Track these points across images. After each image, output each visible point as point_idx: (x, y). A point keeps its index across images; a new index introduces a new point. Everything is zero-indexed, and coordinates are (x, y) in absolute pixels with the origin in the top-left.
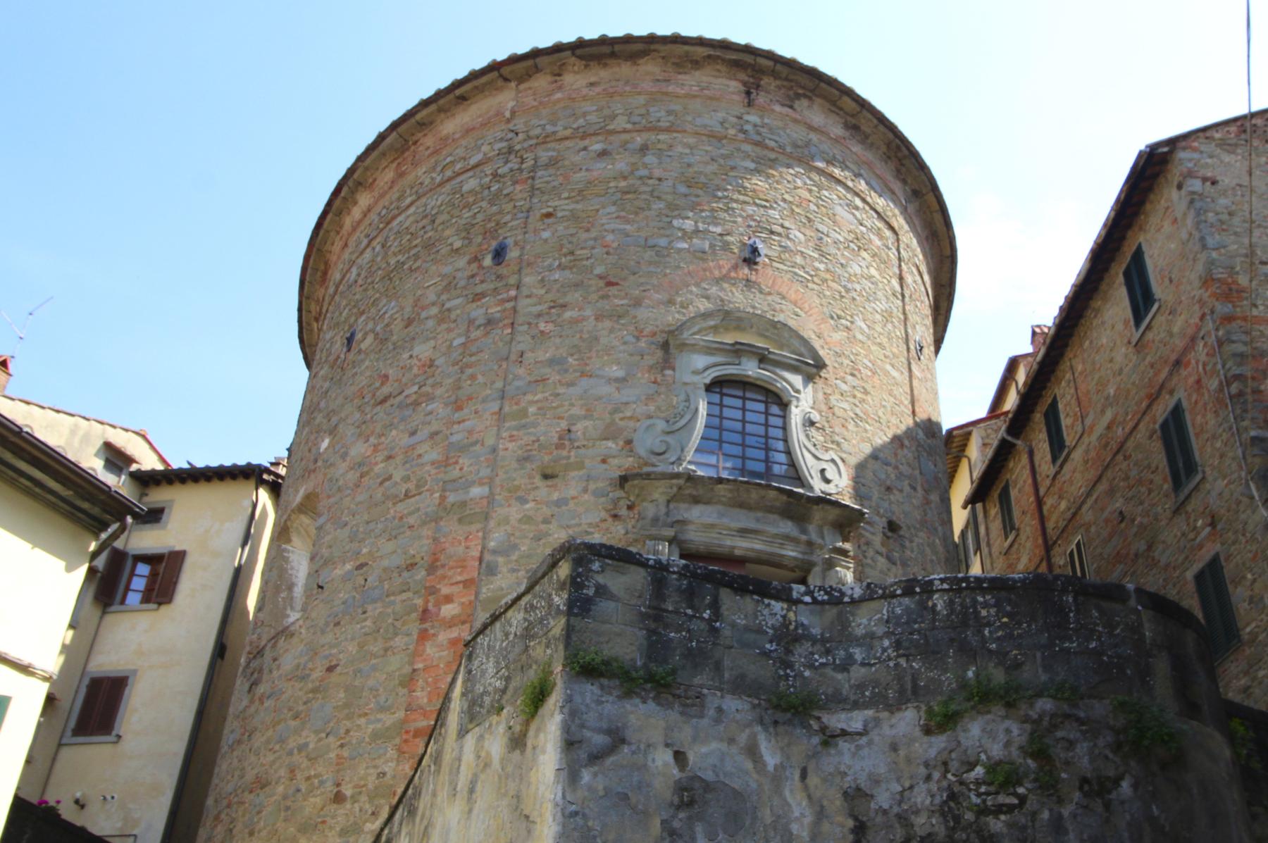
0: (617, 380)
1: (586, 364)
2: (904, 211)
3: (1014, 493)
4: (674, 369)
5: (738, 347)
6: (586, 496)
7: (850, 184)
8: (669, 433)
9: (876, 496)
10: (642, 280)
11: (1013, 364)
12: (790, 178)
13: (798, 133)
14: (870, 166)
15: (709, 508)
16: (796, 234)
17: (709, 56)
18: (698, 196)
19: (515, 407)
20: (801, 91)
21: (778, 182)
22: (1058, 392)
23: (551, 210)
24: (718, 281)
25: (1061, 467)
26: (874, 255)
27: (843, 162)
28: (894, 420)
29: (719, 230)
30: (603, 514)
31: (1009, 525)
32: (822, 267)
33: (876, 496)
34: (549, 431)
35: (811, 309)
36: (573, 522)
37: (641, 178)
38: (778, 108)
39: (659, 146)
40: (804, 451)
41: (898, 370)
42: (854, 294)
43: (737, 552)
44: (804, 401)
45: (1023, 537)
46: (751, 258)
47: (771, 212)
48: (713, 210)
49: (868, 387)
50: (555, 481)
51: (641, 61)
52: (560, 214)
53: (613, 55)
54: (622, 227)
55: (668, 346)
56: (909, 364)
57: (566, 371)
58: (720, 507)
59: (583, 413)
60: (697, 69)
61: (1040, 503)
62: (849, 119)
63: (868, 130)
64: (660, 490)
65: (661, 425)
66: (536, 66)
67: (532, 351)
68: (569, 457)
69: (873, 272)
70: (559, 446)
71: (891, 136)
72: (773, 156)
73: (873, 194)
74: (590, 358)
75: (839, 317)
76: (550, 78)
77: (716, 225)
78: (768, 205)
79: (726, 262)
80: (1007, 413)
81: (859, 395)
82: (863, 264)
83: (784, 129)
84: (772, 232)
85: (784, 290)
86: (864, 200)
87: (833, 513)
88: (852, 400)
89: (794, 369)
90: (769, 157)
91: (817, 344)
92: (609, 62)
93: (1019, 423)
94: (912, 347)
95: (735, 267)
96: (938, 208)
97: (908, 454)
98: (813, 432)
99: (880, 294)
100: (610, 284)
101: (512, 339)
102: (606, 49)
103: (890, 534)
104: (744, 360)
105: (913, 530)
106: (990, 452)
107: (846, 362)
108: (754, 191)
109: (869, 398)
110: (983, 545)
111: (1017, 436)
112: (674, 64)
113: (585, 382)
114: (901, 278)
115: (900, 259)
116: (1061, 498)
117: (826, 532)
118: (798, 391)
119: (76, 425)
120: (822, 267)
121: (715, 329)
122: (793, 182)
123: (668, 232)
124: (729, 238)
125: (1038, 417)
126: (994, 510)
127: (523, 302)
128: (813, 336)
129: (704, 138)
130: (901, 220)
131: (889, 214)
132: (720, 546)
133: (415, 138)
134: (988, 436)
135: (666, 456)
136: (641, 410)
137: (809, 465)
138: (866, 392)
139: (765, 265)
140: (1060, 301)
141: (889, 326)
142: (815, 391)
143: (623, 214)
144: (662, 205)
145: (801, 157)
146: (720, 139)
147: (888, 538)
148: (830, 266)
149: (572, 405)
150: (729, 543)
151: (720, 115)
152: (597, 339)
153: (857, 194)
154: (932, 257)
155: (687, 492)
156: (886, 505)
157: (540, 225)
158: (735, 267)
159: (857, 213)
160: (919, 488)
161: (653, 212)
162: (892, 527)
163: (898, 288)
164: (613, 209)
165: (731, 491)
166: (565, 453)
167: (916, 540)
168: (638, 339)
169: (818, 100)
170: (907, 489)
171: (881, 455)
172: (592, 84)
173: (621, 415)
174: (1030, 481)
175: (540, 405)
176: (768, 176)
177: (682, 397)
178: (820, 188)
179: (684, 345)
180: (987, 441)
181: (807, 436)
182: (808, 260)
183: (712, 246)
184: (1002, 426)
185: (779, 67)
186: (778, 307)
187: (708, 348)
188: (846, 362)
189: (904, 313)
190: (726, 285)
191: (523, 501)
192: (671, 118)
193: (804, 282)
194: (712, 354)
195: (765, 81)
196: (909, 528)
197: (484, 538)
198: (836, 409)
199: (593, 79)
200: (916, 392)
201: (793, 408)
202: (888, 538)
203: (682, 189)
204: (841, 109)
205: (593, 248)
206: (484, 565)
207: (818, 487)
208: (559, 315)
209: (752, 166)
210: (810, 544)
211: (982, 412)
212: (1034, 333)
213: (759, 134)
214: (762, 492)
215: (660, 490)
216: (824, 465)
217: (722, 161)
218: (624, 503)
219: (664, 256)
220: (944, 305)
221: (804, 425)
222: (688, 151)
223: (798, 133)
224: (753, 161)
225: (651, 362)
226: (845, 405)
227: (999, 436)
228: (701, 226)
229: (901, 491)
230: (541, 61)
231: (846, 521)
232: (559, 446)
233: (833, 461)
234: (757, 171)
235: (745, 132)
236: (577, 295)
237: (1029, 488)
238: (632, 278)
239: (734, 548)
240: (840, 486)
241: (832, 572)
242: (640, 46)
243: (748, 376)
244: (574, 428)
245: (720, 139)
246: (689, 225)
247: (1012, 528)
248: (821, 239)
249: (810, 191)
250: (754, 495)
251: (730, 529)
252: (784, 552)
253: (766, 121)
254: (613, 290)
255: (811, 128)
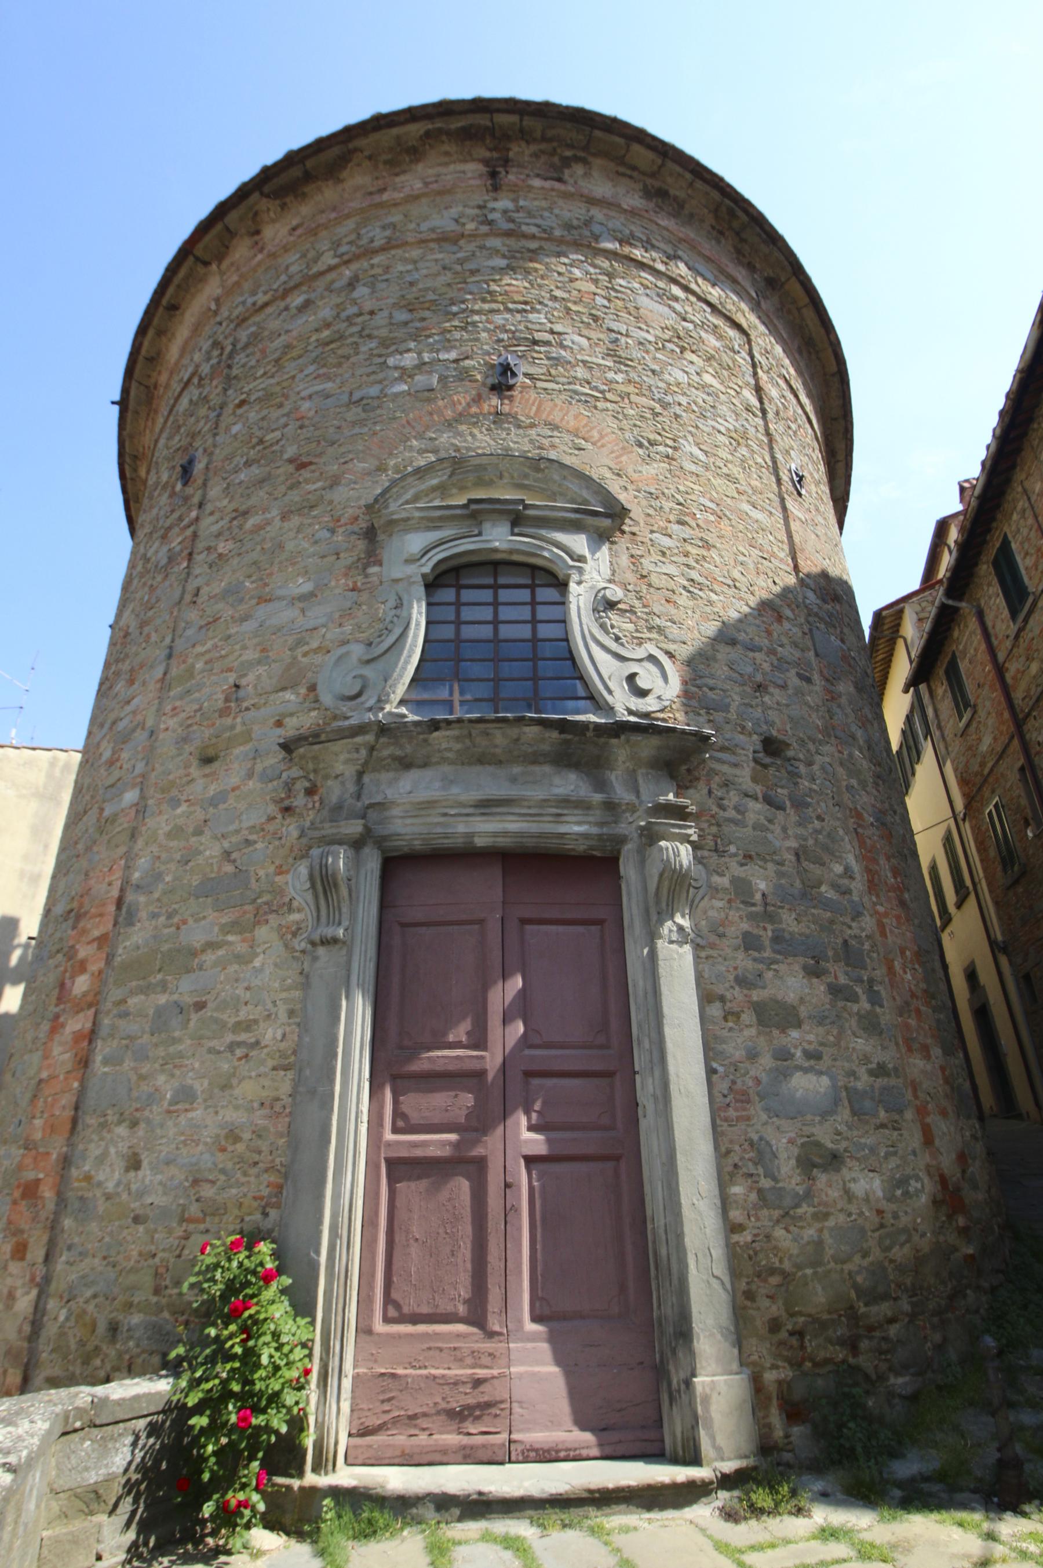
0: (303, 598)
1: (266, 585)
2: (756, 307)
3: (963, 666)
4: (381, 565)
5: (474, 507)
6: (251, 783)
7: (661, 267)
8: (369, 662)
9: (736, 701)
10: (342, 450)
11: (942, 527)
12: (562, 269)
13: (573, 212)
14: (693, 247)
15: (428, 773)
16: (573, 338)
17: (428, 134)
18: (423, 319)
19: (183, 666)
20: (568, 153)
21: (542, 277)
22: (1008, 529)
23: (244, 396)
24: (450, 424)
25: (1026, 620)
26: (710, 359)
27: (648, 241)
28: (761, 582)
29: (453, 355)
30: (272, 809)
31: (962, 702)
32: (619, 377)
33: (736, 701)
34: (213, 691)
35: (602, 437)
36: (232, 828)
37: (348, 319)
38: (537, 183)
39: (373, 272)
40: (595, 649)
41: (763, 510)
42: (678, 410)
43: (480, 842)
44: (594, 571)
45: (982, 713)
46: (502, 381)
47: (532, 317)
48: (446, 331)
49: (711, 538)
50: (216, 765)
51: (344, 174)
52: (253, 398)
53: (308, 177)
54: (321, 387)
55: (374, 534)
56: (782, 500)
57: (241, 600)
58: (447, 769)
59: (257, 656)
60: (418, 161)
61: (1000, 671)
62: (649, 181)
63: (682, 194)
64: (342, 757)
65: (357, 650)
66: (227, 229)
67: (208, 585)
68: (233, 727)
69: (708, 378)
70: (224, 712)
71: (715, 195)
72: (533, 245)
73: (700, 280)
74: (271, 574)
75: (653, 443)
76: (247, 242)
77: (448, 350)
78: (527, 306)
79: (462, 397)
80: (941, 581)
81: (694, 551)
82: (691, 369)
83: (550, 209)
84: (535, 342)
85: (556, 417)
86: (686, 289)
87: (648, 747)
88: (682, 559)
89: (574, 526)
90: (524, 248)
91: (614, 487)
92: (307, 189)
93: (960, 583)
94: (785, 477)
95: (478, 399)
96: (807, 300)
97: (791, 628)
98: (613, 617)
99: (723, 409)
100: (303, 466)
101: (188, 574)
102: (296, 172)
103: (767, 760)
104: (487, 526)
105: (811, 747)
106: (927, 626)
107: (668, 505)
108: (506, 293)
109: (713, 553)
110: (933, 728)
111: (960, 598)
112: (385, 162)
113: (262, 611)
114: (758, 390)
115: (754, 366)
116: (1029, 659)
117: (641, 781)
118: (581, 559)
119: (55, 758)
120: (619, 377)
121: (442, 489)
122: (575, 275)
123: (381, 376)
124: (468, 363)
125: (985, 568)
126: (942, 689)
127: (206, 521)
128: (608, 475)
129: (432, 245)
130: (753, 318)
131: (729, 307)
132: (446, 836)
133: (153, 381)
134: (923, 610)
135: (362, 699)
136: (334, 633)
137: (604, 668)
138: (707, 545)
139: (524, 387)
140: (999, 402)
141: (744, 451)
142: (613, 555)
143: (322, 371)
144: (373, 344)
145: (580, 240)
146: (455, 242)
147: (765, 766)
148: (633, 375)
149: (244, 648)
150: (461, 828)
151: (454, 212)
152: (281, 546)
153: (674, 281)
154: (812, 379)
155: (385, 753)
156: (758, 713)
157: (231, 419)
158: (478, 399)
159: (677, 306)
160: (816, 677)
161: (361, 357)
162: (772, 747)
163: (754, 401)
164: (311, 368)
165: (457, 739)
166: (228, 721)
167: (818, 758)
168: (333, 531)
169: (597, 162)
170: (794, 681)
171: (742, 637)
172: (294, 229)
173: (306, 648)
174: (983, 646)
175: (207, 657)
176: (527, 272)
177: (391, 603)
178: (611, 276)
179: (392, 523)
180: (922, 615)
181: (603, 626)
182: (596, 373)
183: (442, 379)
184: (939, 594)
185: (528, 122)
186: (546, 442)
187: (431, 519)
188: (668, 505)
189: (768, 433)
190: (463, 428)
191: (175, 803)
192: (388, 233)
193: (588, 401)
194: (428, 529)
195: (517, 150)
196: (802, 742)
197: (127, 867)
198: (654, 579)
199: (294, 223)
200: (797, 539)
201: (573, 586)
202: (765, 766)
203: (402, 316)
204: (634, 168)
205: (286, 425)
206: (124, 910)
207: (622, 703)
208: (240, 527)
209: (503, 263)
210: (611, 806)
211: (916, 585)
212: (962, 490)
213: (512, 220)
214: (513, 732)
215: (342, 757)
216: (634, 668)
217: (458, 268)
218: (301, 785)
219: (374, 409)
220: (840, 446)
221: (595, 610)
222: (410, 267)
223: (573, 212)
224: (504, 257)
225: (350, 560)
226: (672, 569)
227: (937, 603)
228: (426, 357)
229: (784, 687)
230: (232, 218)
231: (677, 755)
232: (224, 712)
233: (652, 658)
234: (511, 268)
235: (490, 223)
236: (261, 493)
237: (982, 654)
238: (330, 450)
239: (471, 835)
240: (664, 693)
241: (654, 850)
242: (336, 151)
243: (495, 550)
244: (243, 682)
245: (455, 242)
246: (409, 360)
247: (967, 705)
248: (617, 340)
249: (596, 282)
250: (500, 738)
251: (462, 805)
252: (563, 829)
253: (521, 203)
254: (305, 474)
255: (592, 201)
